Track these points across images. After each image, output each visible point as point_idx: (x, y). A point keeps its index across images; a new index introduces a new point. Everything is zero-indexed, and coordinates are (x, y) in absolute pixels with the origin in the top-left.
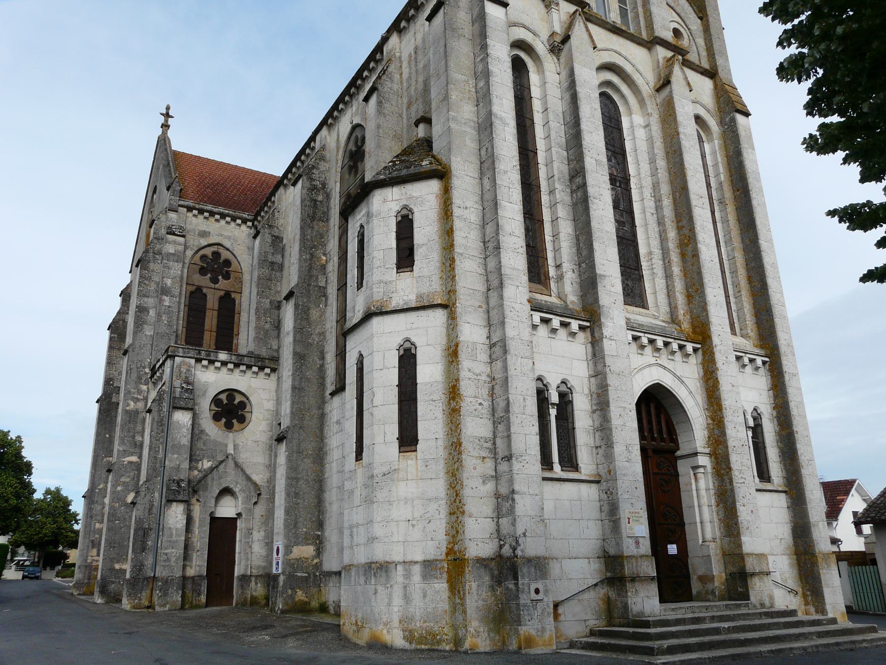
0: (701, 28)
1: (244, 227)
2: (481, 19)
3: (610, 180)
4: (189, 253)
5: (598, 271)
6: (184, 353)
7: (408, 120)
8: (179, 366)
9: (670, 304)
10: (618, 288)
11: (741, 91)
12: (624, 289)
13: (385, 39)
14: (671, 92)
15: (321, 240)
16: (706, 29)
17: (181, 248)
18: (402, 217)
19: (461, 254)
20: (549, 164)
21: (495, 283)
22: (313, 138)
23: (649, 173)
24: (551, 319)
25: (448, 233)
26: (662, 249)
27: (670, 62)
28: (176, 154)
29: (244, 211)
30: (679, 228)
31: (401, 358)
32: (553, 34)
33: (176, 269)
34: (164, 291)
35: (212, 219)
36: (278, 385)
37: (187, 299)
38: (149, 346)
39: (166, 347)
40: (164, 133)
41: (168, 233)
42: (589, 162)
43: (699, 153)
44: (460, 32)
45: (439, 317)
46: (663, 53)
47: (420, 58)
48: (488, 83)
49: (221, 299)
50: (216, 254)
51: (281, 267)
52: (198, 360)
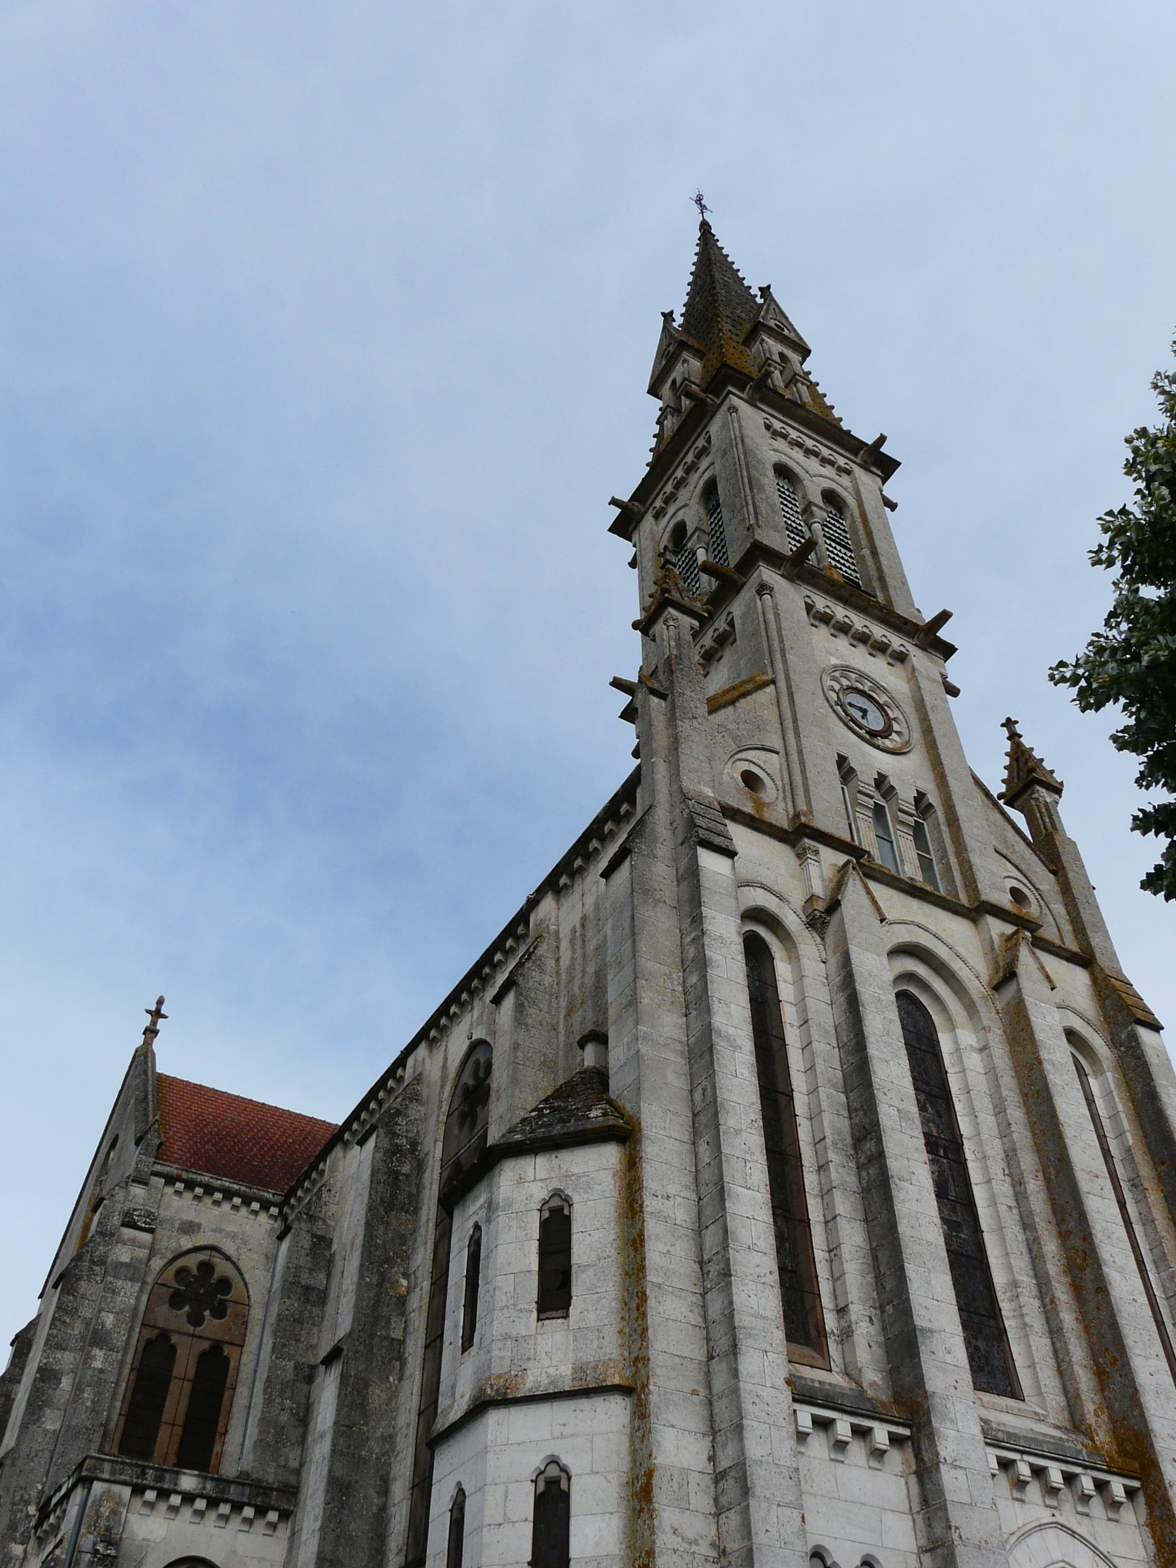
0: (1057, 888)
1: (263, 1217)
2: (691, 876)
3: (926, 1144)
4: (157, 1263)
5: (918, 1322)
6: (113, 1472)
7: (567, 1035)
8: (98, 1503)
9: (1065, 1391)
10: (959, 1355)
11: (1138, 988)
12: (971, 1357)
13: (532, 903)
14: (1019, 990)
15: (402, 1244)
16: (1066, 889)
17: (143, 1253)
18: (551, 1210)
19: (659, 1286)
20: (815, 1116)
21: (722, 1344)
22: (401, 1062)
23: (995, 1132)
24: (833, 1421)
25: (634, 1243)
26: (1036, 1276)
27: (1011, 942)
28: (162, 1080)
29: (267, 1187)
30: (1063, 1236)
31: (539, 1500)
32: (812, 898)
33: (128, 1294)
34: (98, 1338)
35: (208, 1201)
36: (290, 1550)
37: (138, 1357)
38: (47, 1454)
39: (80, 1458)
40: (147, 1043)
41: (124, 1225)
42: (887, 1114)
43: (1081, 1095)
44: (658, 895)
45: (612, 1413)
46: (997, 928)
47: (590, 934)
48: (704, 978)
49: (203, 1357)
50: (206, 1268)
51: (322, 1298)
52: (138, 1490)
